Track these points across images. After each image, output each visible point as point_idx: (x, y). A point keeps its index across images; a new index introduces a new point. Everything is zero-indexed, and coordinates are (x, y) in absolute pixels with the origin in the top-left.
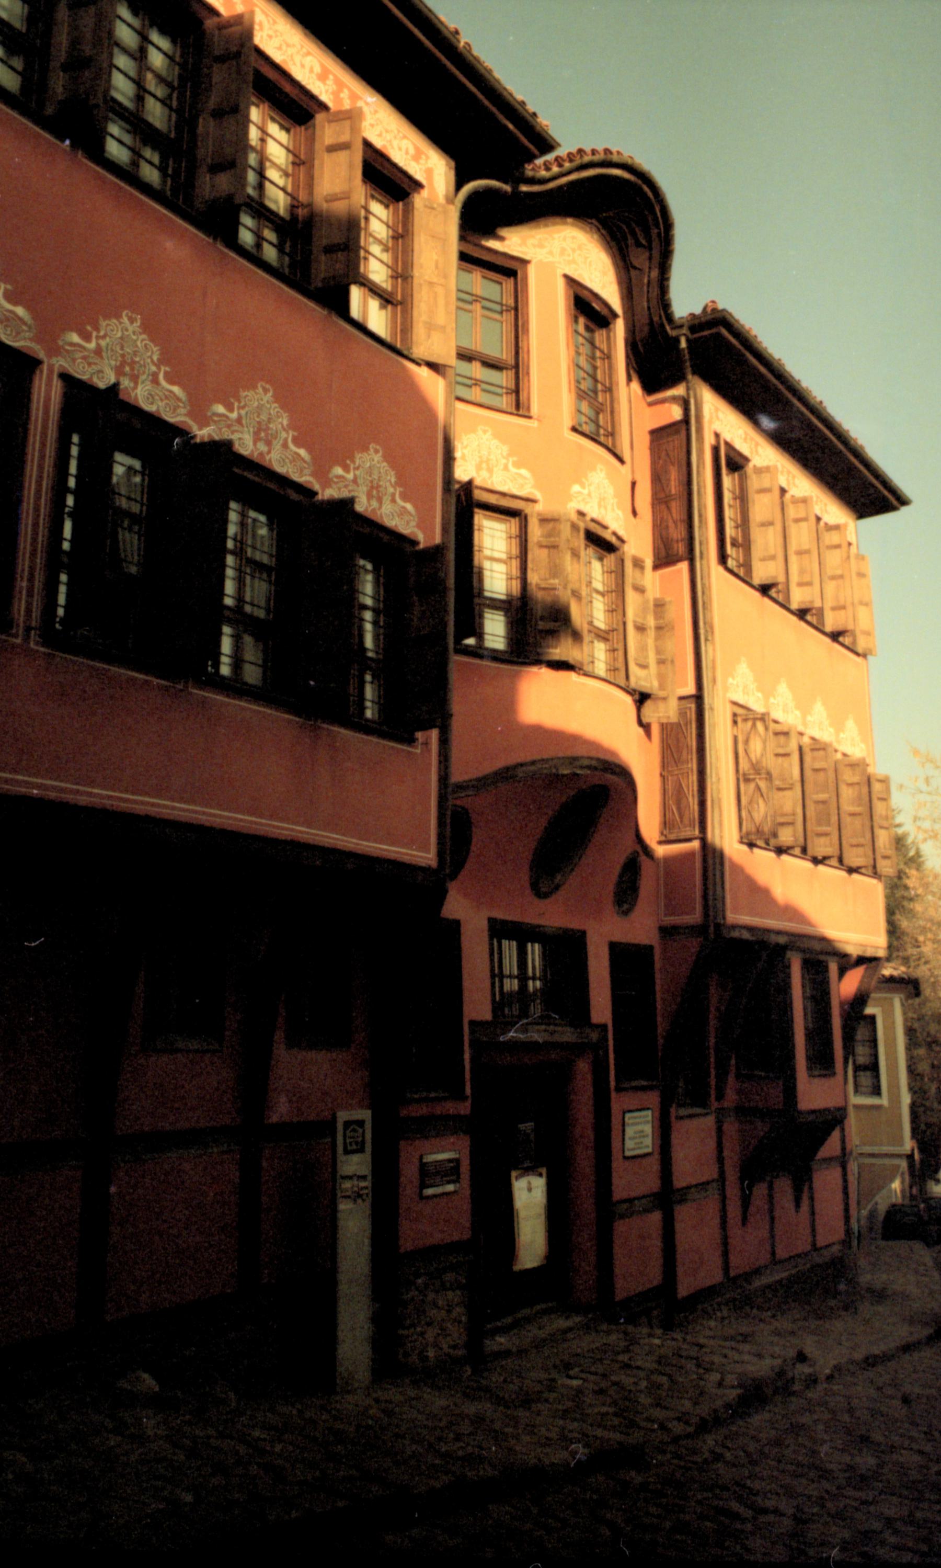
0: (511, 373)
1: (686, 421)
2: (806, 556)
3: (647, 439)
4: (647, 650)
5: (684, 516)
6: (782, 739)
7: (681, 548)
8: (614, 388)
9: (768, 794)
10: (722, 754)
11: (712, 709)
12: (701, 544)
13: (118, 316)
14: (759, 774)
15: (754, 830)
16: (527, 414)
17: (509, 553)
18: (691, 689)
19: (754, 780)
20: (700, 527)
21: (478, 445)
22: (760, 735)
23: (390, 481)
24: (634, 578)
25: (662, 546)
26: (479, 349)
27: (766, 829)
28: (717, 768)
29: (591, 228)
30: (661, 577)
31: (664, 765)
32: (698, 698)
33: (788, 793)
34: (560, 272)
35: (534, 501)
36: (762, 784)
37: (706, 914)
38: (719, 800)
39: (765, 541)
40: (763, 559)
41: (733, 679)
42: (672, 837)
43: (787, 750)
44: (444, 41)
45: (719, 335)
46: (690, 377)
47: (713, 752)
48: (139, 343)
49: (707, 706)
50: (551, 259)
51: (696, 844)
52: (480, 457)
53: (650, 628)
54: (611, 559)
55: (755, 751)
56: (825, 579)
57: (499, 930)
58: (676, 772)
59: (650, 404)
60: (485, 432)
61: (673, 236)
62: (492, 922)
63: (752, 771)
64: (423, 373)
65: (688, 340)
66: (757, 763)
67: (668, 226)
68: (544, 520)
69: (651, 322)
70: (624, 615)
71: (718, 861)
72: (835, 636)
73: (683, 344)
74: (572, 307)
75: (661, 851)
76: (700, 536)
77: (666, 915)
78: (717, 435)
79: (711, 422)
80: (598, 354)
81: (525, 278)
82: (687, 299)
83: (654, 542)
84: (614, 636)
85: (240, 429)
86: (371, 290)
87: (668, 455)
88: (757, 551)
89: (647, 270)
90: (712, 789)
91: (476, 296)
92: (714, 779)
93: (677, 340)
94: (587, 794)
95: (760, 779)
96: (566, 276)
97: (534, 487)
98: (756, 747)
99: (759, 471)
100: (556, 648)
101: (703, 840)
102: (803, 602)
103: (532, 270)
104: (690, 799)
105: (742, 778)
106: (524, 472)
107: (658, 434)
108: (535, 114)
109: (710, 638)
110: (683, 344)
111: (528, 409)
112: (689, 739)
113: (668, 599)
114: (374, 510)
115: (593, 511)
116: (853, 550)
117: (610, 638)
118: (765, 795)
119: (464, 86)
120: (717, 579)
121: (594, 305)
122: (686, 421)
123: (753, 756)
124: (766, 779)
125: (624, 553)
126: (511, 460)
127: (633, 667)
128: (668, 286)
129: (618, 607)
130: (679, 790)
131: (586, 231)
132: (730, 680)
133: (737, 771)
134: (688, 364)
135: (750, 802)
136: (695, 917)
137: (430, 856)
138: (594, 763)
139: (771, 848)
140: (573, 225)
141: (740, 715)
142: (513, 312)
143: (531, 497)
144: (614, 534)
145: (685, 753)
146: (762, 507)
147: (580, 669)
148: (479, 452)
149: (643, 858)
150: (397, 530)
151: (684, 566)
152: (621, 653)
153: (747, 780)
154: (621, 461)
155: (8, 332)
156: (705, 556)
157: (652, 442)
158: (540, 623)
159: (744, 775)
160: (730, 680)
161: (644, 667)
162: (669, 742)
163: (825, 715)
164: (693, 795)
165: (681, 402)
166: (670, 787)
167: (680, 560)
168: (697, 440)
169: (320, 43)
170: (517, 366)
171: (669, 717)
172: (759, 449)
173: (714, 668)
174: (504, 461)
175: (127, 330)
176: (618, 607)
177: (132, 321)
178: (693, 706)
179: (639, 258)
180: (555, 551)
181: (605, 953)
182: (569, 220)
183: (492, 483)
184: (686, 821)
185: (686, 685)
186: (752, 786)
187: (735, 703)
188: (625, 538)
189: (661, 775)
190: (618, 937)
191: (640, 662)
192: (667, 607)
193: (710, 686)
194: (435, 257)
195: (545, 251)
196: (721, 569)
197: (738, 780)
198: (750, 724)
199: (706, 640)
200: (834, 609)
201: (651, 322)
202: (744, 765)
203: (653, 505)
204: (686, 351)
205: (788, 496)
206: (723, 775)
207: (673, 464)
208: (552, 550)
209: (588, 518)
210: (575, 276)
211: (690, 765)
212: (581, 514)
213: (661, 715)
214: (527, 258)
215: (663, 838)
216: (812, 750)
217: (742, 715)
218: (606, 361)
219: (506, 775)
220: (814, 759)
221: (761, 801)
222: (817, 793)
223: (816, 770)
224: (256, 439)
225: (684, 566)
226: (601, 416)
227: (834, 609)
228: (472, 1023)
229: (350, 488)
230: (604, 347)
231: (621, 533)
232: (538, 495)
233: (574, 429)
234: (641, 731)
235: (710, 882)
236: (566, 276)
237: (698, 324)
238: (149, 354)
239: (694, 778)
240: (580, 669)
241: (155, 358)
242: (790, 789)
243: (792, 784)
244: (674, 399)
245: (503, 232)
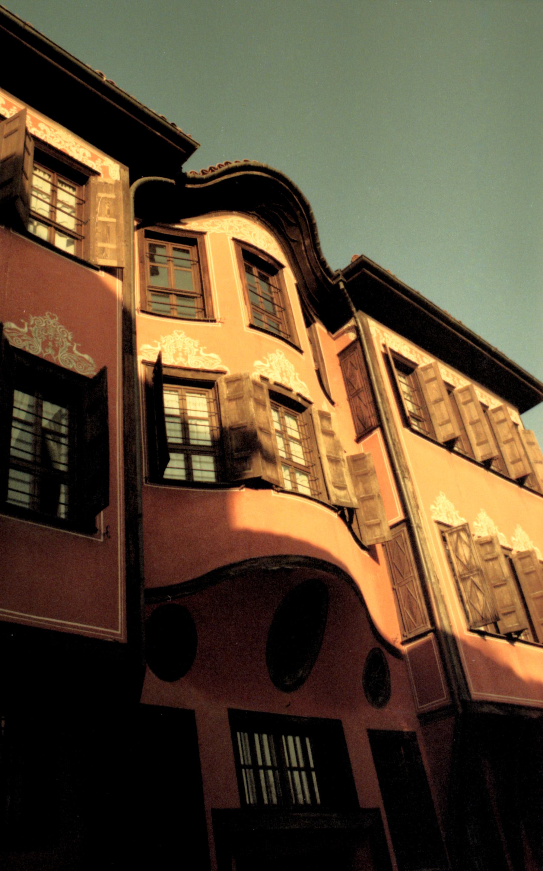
0: (200, 300)
1: (359, 339)
2: (479, 424)
3: (337, 360)
4: (343, 476)
5: (371, 399)
6: (488, 548)
7: (373, 421)
8: (288, 308)
9: (482, 586)
10: (436, 561)
11: (419, 527)
12: (385, 413)
13: (275, 352)
14: (472, 572)
15: (479, 618)
16: (212, 319)
17: (209, 412)
18: (400, 516)
19: (469, 578)
20: (382, 402)
21: (175, 342)
22: (465, 543)
23: (67, 338)
24: (322, 425)
25: (358, 422)
26: (173, 287)
27: (489, 616)
28: (434, 572)
29: (252, 217)
30: (364, 445)
31: (393, 580)
32: (407, 521)
33: (504, 588)
34: (229, 238)
35: (224, 373)
36: (477, 580)
37: (451, 694)
38: (442, 597)
39: (441, 412)
40: (441, 425)
41: (435, 505)
42: (411, 636)
43: (495, 555)
44: (94, 81)
45: (365, 273)
46: (356, 314)
47: (427, 559)
48: (58, 330)
49: (414, 525)
50: (222, 231)
51: (431, 636)
52: (177, 349)
53: (343, 460)
54: (302, 416)
55: (464, 555)
56: (501, 444)
57: (243, 722)
58: (404, 583)
59: (334, 339)
60: (179, 334)
61: (312, 213)
62: (233, 714)
63: (465, 572)
64: (102, 274)
65: (345, 284)
66: (468, 563)
67: (307, 208)
68: (229, 382)
69: (317, 279)
70: (319, 453)
71: (451, 645)
72: (520, 482)
73: (342, 286)
74: (242, 259)
75: (405, 648)
76: (384, 408)
77: (421, 703)
78: (384, 346)
79: (378, 338)
80: (272, 289)
81: (203, 243)
82: (338, 259)
83: (354, 423)
84: (312, 469)
85: (30, 338)
86: (56, 229)
87: (352, 364)
88: (436, 422)
89: (302, 241)
90: (433, 589)
91: (169, 257)
92: (433, 580)
93: (337, 285)
94: (309, 591)
95: (473, 576)
96: (234, 239)
97: (222, 363)
98: (464, 551)
99: (425, 369)
100: (250, 469)
101: (435, 630)
102: (485, 456)
103: (207, 239)
104: (419, 601)
105: (459, 580)
106: (213, 355)
107: (342, 354)
108: (173, 125)
109: (406, 475)
110: (342, 286)
111: (213, 316)
112: (407, 554)
113: (366, 453)
114: (50, 355)
115: (274, 377)
116: (520, 428)
117: (311, 471)
118: (481, 588)
119: (114, 107)
120: (407, 440)
121: (260, 256)
122: (359, 339)
123: (463, 560)
124: (478, 574)
125: (311, 410)
126: (201, 348)
127: (331, 488)
128: (320, 249)
129: (311, 449)
130: (409, 596)
131: (249, 219)
132: (432, 507)
133: (454, 575)
134: (350, 300)
135: (470, 597)
136: (444, 700)
137: (119, 632)
138: (302, 560)
139: (501, 635)
140: (237, 215)
141: (447, 531)
142: (197, 264)
143: (220, 369)
144: (299, 395)
145: (407, 565)
146: (432, 392)
147: (277, 486)
148: (175, 346)
149: (389, 657)
150: (74, 371)
151: (377, 432)
152: (321, 481)
153: (464, 580)
154: (301, 352)
155: (81, 367)
156: (391, 420)
157: (341, 360)
158: (235, 454)
159: (461, 575)
160: (432, 507)
161: (342, 488)
162: (394, 561)
163: (527, 537)
164: (420, 597)
165: (354, 330)
166: (401, 597)
167: (374, 429)
168: (367, 343)
169: (8, 93)
170: (202, 295)
171: (384, 537)
172: (424, 359)
173: (415, 498)
174: (196, 350)
175: (49, 323)
176: (311, 449)
177: (280, 353)
178: (405, 529)
179: (294, 234)
180: (241, 401)
181: (364, 740)
182: (234, 212)
183: (188, 364)
184: (419, 618)
185: (397, 515)
186: (469, 583)
187: (439, 523)
188: (312, 400)
189: (394, 589)
190: (375, 726)
191: (337, 485)
192: (368, 458)
193: (415, 512)
194: (107, 207)
195: (216, 228)
196: (407, 431)
197: (457, 582)
198: (455, 536)
199: (404, 477)
200: (513, 463)
201: (317, 279)
202: (458, 569)
203: (349, 400)
204: (345, 291)
205: (455, 391)
206: (441, 577)
207: (357, 369)
208: (238, 401)
209: (272, 382)
210: (239, 237)
211: (412, 575)
212: (264, 379)
213: (378, 537)
214: (204, 230)
215: (405, 639)
216: (520, 559)
217: (446, 531)
218: (279, 294)
219: (218, 575)
220: (523, 566)
221: (479, 594)
222: (533, 592)
223: (527, 574)
224: (45, 345)
225: (377, 432)
226: (280, 326)
227: (513, 463)
228: (215, 812)
229: (24, 338)
230: (277, 285)
231: (307, 396)
232: (225, 368)
233: (252, 326)
234: (365, 553)
235: (449, 666)
236: (234, 239)
237: (349, 272)
238: (66, 336)
239: (418, 582)
240: (277, 486)
241: (70, 338)
242: (505, 584)
243: (505, 580)
244: (349, 329)
245: (183, 221)
